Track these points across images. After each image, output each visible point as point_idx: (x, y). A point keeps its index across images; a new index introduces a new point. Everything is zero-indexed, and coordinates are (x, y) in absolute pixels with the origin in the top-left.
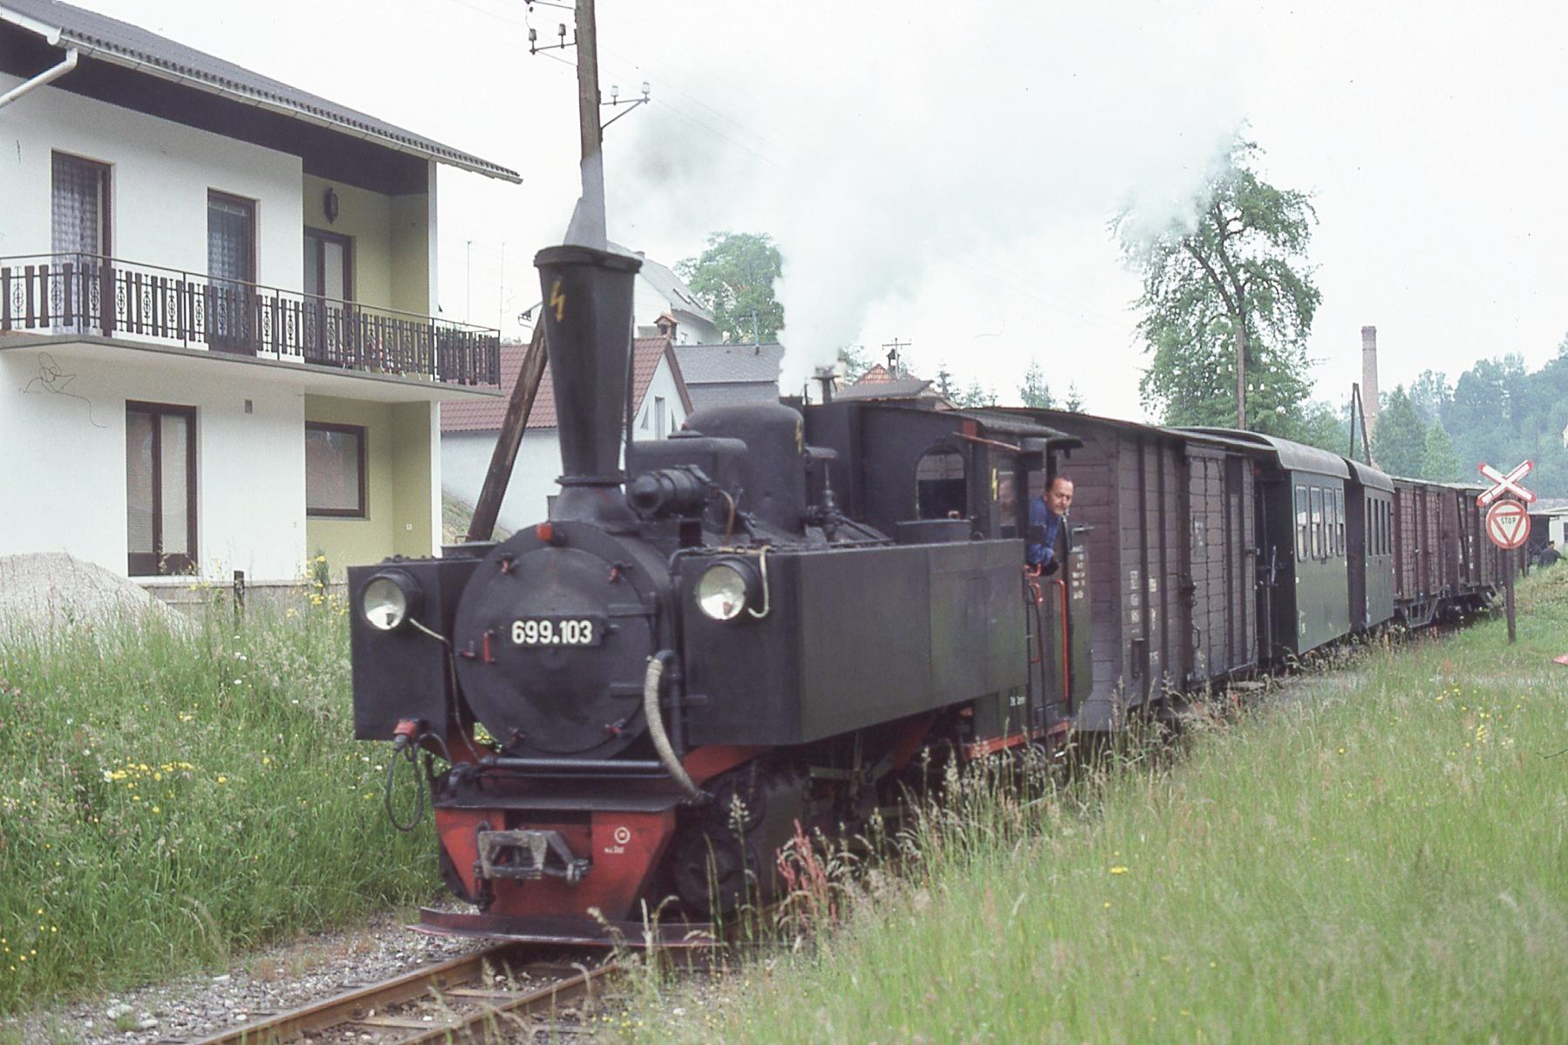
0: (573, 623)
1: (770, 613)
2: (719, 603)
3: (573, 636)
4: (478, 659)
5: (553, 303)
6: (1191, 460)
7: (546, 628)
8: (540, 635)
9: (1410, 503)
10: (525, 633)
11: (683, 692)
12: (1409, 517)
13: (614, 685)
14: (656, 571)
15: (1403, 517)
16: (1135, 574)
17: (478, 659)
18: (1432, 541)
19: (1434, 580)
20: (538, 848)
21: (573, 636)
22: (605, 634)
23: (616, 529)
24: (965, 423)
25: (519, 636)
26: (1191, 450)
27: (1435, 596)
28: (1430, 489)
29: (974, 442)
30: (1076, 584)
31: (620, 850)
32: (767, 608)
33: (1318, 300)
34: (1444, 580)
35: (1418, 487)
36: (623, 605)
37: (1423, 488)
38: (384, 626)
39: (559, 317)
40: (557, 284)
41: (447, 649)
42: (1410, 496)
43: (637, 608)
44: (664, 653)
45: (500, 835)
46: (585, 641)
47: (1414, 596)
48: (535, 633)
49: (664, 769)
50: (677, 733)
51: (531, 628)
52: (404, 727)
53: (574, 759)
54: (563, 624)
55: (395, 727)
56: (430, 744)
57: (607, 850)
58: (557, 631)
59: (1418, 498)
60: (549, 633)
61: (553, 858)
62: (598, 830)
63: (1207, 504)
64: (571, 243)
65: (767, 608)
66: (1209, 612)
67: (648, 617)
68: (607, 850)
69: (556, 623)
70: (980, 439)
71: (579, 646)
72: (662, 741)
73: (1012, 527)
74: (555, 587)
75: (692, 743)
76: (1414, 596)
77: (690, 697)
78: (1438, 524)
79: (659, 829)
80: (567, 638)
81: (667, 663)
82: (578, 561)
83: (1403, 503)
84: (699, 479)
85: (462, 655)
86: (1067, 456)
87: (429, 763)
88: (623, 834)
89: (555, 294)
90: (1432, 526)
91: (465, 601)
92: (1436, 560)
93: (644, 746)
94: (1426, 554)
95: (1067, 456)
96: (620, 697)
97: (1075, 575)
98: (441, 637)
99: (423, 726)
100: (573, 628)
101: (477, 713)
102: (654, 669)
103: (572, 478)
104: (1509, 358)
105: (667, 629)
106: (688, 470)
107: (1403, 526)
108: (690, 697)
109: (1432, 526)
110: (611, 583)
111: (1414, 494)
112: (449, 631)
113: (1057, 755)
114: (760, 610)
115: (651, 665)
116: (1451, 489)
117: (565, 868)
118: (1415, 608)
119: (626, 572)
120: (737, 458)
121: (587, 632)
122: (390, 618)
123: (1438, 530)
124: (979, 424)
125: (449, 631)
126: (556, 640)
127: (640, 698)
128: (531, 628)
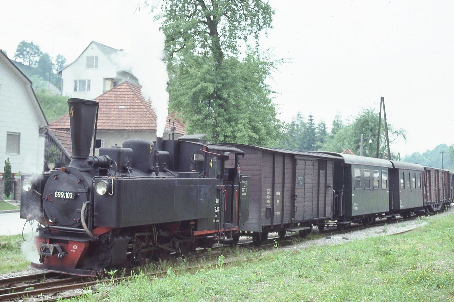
0: (69, 193)
1: (113, 194)
5: (71, 112)
6: (297, 160)
9: (434, 175)
10: (58, 195)
12: (433, 179)
13: (77, 209)
14: (89, 181)
15: (431, 179)
16: (269, 191)
18: (441, 186)
19: (441, 197)
20: (51, 248)
22: (76, 196)
23: (81, 169)
26: (296, 157)
27: (442, 202)
28: (440, 171)
29: (206, 152)
31: (74, 251)
32: (113, 193)
34: (445, 198)
35: (435, 170)
36: (80, 189)
37: (438, 171)
39: (72, 116)
40: (72, 108)
41: (42, 197)
42: (434, 173)
46: (71, 198)
47: (435, 202)
48: (60, 195)
53: (70, 227)
57: (72, 251)
58: (65, 195)
59: (436, 173)
60: (63, 195)
62: (70, 245)
63: (305, 172)
65: (113, 193)
66: (304, 202)
67: (86, 193)
68: (72, 251)
69: (65, 192)
71: (69, 199)
72: (84, 224)
74: (66, 183)
75: (95, 225)
76: (435, 202)
78: (443, 181)
79: (83, 247)
80: (67, 197)
81: (88, 205)
83: (431, 174)
84: (107, 159)
86: (243, 157)
88: (75, 247)
89: (71, 110)
90: (441, 182)
91: (46, 186)
92: (442, 191)
94: (439, 190)
97: (243, 189)
98: (40, 194)
103: (74, 156)
106: (105, 156)
107: (431, 181)
109: (441, 182)
110: (78, 183)
111: (435, 172)
112: (42, 192)
114: (111, 193)
115: (84, 205)
116: (446, 171)
118: (435, 205)
119: (82, 181)
121: (71, 196)
123: (443, 183)
125: (42, 192)
126: (64, 197)
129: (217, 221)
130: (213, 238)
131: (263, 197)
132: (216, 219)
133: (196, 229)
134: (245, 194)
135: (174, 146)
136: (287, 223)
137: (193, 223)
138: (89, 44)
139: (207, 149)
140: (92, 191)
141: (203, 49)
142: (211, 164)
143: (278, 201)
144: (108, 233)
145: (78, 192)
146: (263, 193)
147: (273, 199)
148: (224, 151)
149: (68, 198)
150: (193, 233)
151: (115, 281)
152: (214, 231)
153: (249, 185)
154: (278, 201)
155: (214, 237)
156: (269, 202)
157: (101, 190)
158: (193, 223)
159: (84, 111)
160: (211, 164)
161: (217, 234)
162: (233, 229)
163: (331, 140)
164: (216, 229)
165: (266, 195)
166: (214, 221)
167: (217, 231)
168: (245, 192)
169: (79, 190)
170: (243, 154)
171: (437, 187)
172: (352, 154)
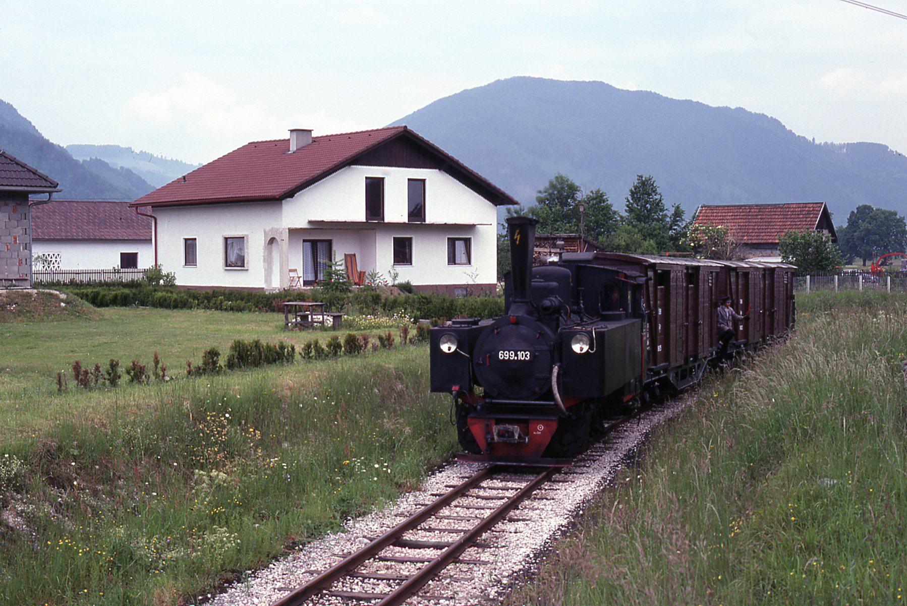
0: (186, 278)
3: (522, 357)
7: (512, 354)
8: (509, 356)
10: (503, 355)
20: (516, 431)
21: (522, 357)
24: (620, 274)
25: (501, 356)
29: (623, 281)
33: (628, 201)
38: (447, 351)
41: (471, 360)
43: (546, 347)
48: (508, 355)
49: (557, 405)
51: (506, 354)
52: (455, 388)
54: (519, 353)
55: (451, 388)
58: (516, 355)
60: (513, 355)
62: (531, 426)
64: (300, 146)
70: (626, 280)
72: (558, 396)
73: (383, 219)
79: (554, 426)
80: (520, 357)
81: (560, 368)
85: (477, 363)
88: (541, 427)
100: (523, 354)
104: (557, 178)
112: (470, 353)
121: (528, 356)
124: (625, 274)
128: (506, 354)
135: (376, 255)
138: (158, 254)
141: (119, 382)
149: (523, 359)
163: (583, 254)
171: (690, 319)
172: (390, 276)
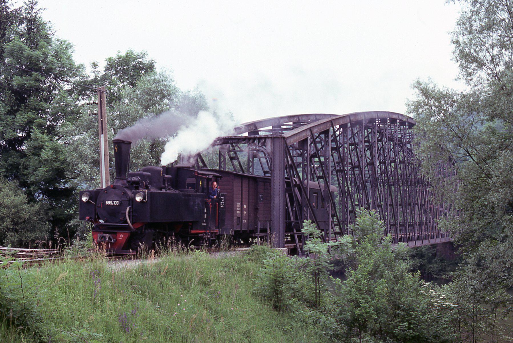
2: (138, 199)
4: (100, 207)
10: (108, 203)
11: (133, 213)
14: (129, 193)
16: (239, 204)
17: (100, 207)
22: (121, 203)
26: (258, 179)
30: (221, 204)
41: (95, 205)
44: (130, 206)
45: (102, 234)
49: (129, 226)
50: (131, 220)
52: (88, 218)
56: (92, 221)
58: (113, 203)
61: (110, 238)
62: (118, 235)
72: (128, 221)
74: (113, 195)
77: (134, 214)
79: (127, 235)
80: (115, 204)
81: (130, 208)
82: (117, 191)
86: (221, 179)
87: (92, 225)
88: (122, 236)
93: (126, 222)
95: (221, 179)
96: (122, 214)
99: (91, 218)
101: (100, 216)
102: (128, 209)
105: (131, 202)
108: (134, 214)
112: (96, 202)
113: (411, 313)
117: (112, 240)
119: (125, 194)
120: (148, 176)
122: (86, 200)
127: (125, 214)
129: (205, 224)
130: (203, 236)
131: (235, 209)
132: (204, 223)
133: (192, 229)
134: (223, 206)
136: (251, 229)
137: (191, 224)
139: (198, 173)
140: (132, 200)
142: (201, 183)
143: (245, 213)
144: (142, 227)
145: (122, 201)
146: (235, 205)
147: (242, 211)
148: (209, 175)
150: (191, 231)
151: (8, 310)
152: (203, 232)
153: (225, 200)
154: (245, 213)
155: (204, 236)
156: (238, 212)
157: (138, 199)
158: (191, 224)
159: (124, 147)
160: (201, 183)
161: (206, 233)
162: (215, 231)
164: (204, 230)
165: (237, 207)
166: (203, 224)
167: (205, 231)
168: (223, 205)
169: (123, 199)
170: (221, 177)
